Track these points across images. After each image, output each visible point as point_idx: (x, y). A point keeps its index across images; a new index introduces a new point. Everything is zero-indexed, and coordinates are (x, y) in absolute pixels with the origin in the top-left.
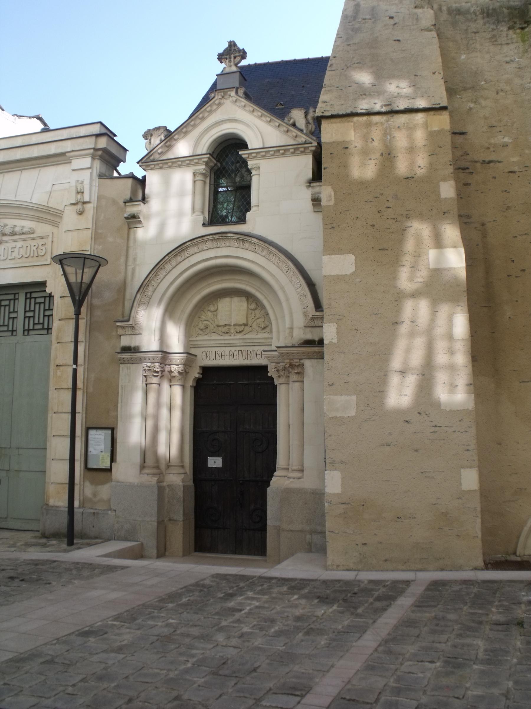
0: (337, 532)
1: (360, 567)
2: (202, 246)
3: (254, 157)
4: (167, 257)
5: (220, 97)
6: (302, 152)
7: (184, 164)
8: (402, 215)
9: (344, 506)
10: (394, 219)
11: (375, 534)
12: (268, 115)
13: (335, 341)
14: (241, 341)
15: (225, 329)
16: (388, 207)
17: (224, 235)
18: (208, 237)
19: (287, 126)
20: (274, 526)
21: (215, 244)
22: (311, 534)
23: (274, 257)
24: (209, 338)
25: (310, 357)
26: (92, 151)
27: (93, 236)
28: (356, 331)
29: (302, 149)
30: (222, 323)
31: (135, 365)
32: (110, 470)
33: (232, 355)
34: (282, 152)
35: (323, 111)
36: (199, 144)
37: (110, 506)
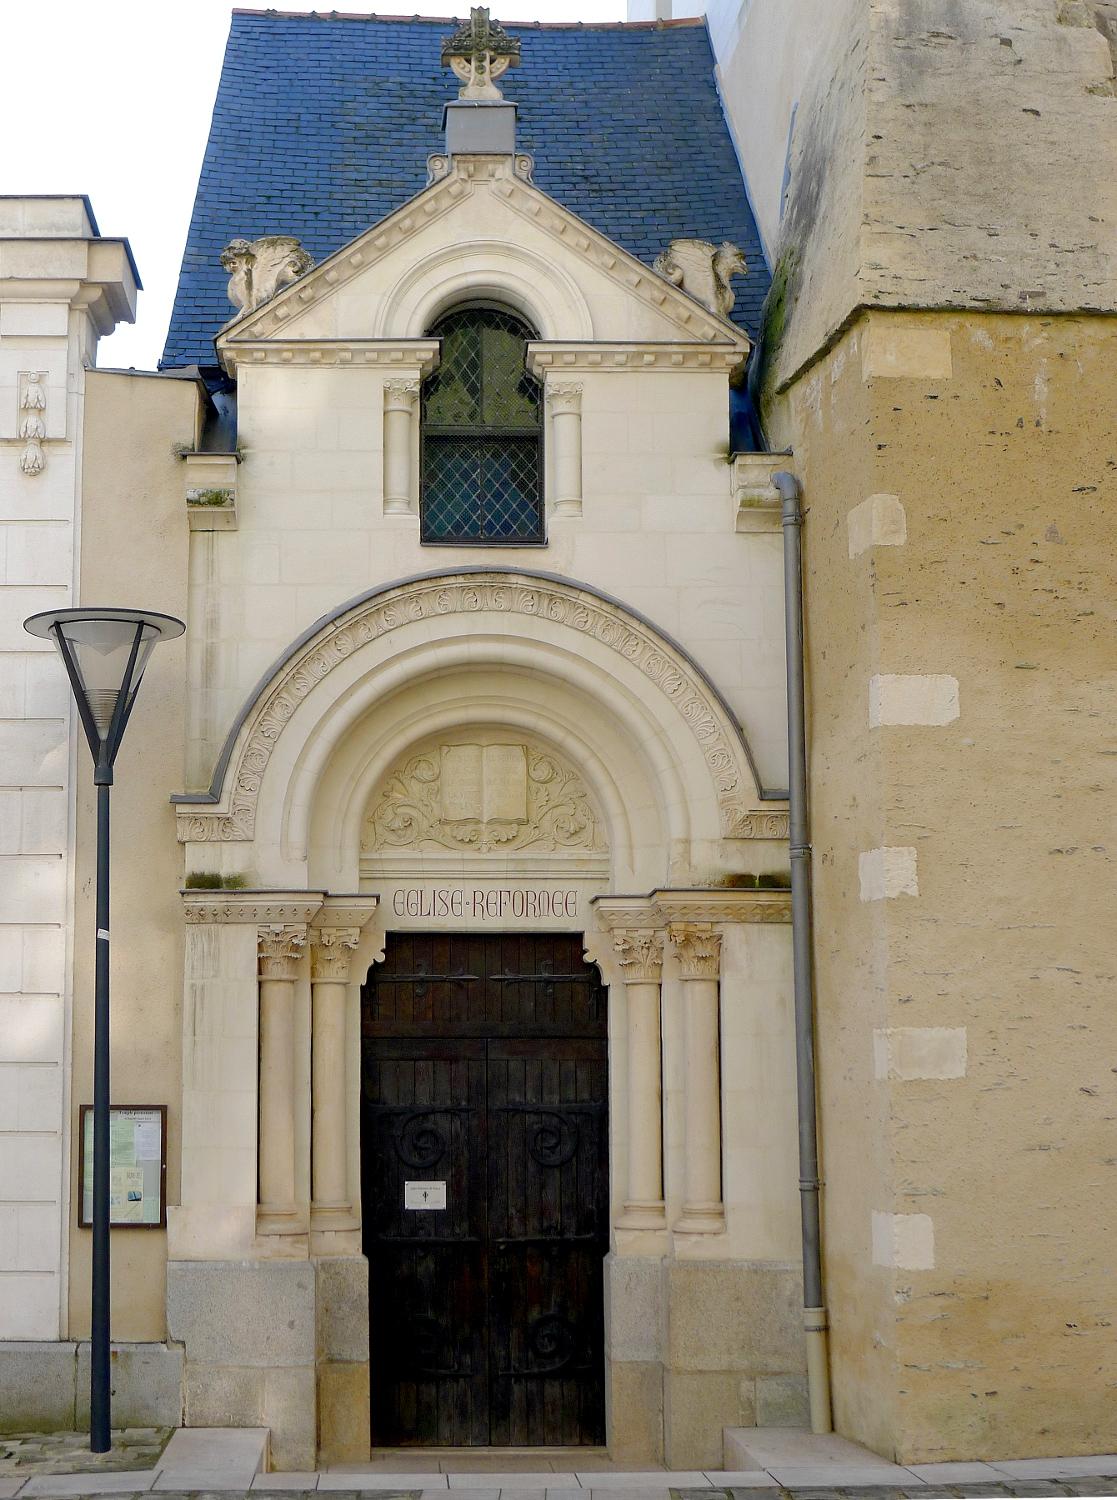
0: (925, 1366)
1: (983, 1452)
2: (429, 604)
3: (595, 364)
4: (331, 628)
5: (464, 175)
6: (703, 365)
7: (359, 359)
8: (1069, 582)
9: (941, 1301)
10: (1051, 591)
11: (1016, 1369)
12: (612, 250)
13: (913, 891)
14: (511, 867)
15: (465, 832)
16: (1037, 561)
17: (499, 578)
18: (452, 580)
19: (665, 288)
20: (631, 1362)
21: (468, 600)
22: (753, 1379)
23: (639, 649)
24: (477, 856)
25: (740, 917)
26: (76, 286)
27: (79, 544)
28: (961, 868)
29: (707, 358)
30: (455, 814)
31: (234, 927)
32: (162, 1225)
33: (481, 903)
34: (648, 358)
35: (875, 292)
36: (398, 304)
37: (166, 1332)
